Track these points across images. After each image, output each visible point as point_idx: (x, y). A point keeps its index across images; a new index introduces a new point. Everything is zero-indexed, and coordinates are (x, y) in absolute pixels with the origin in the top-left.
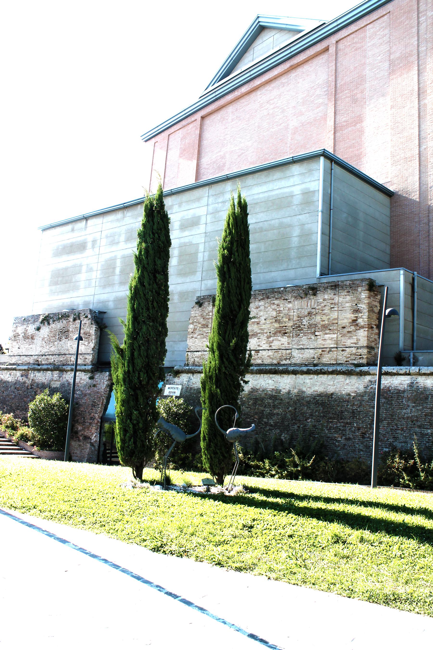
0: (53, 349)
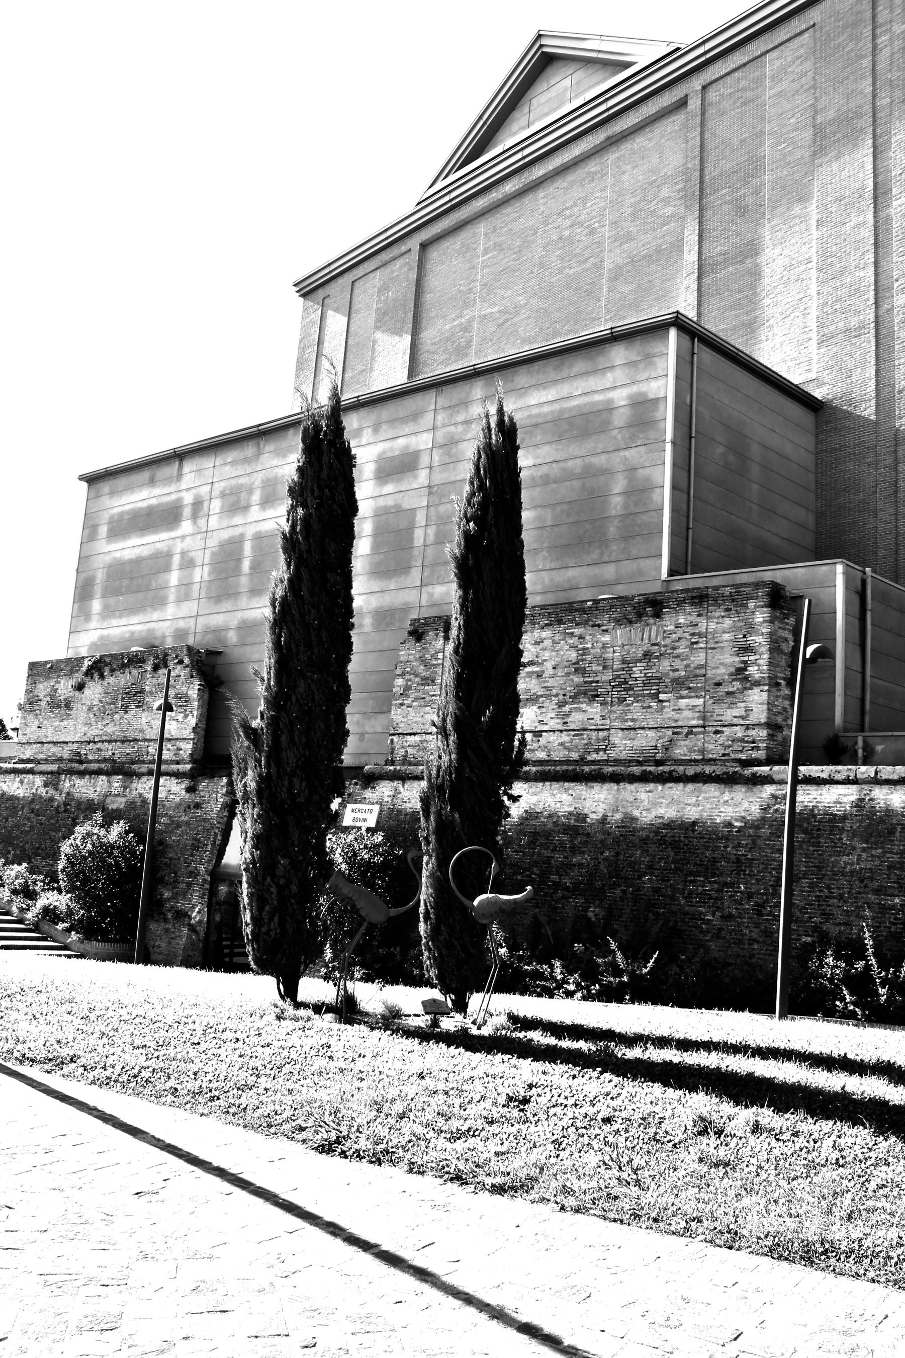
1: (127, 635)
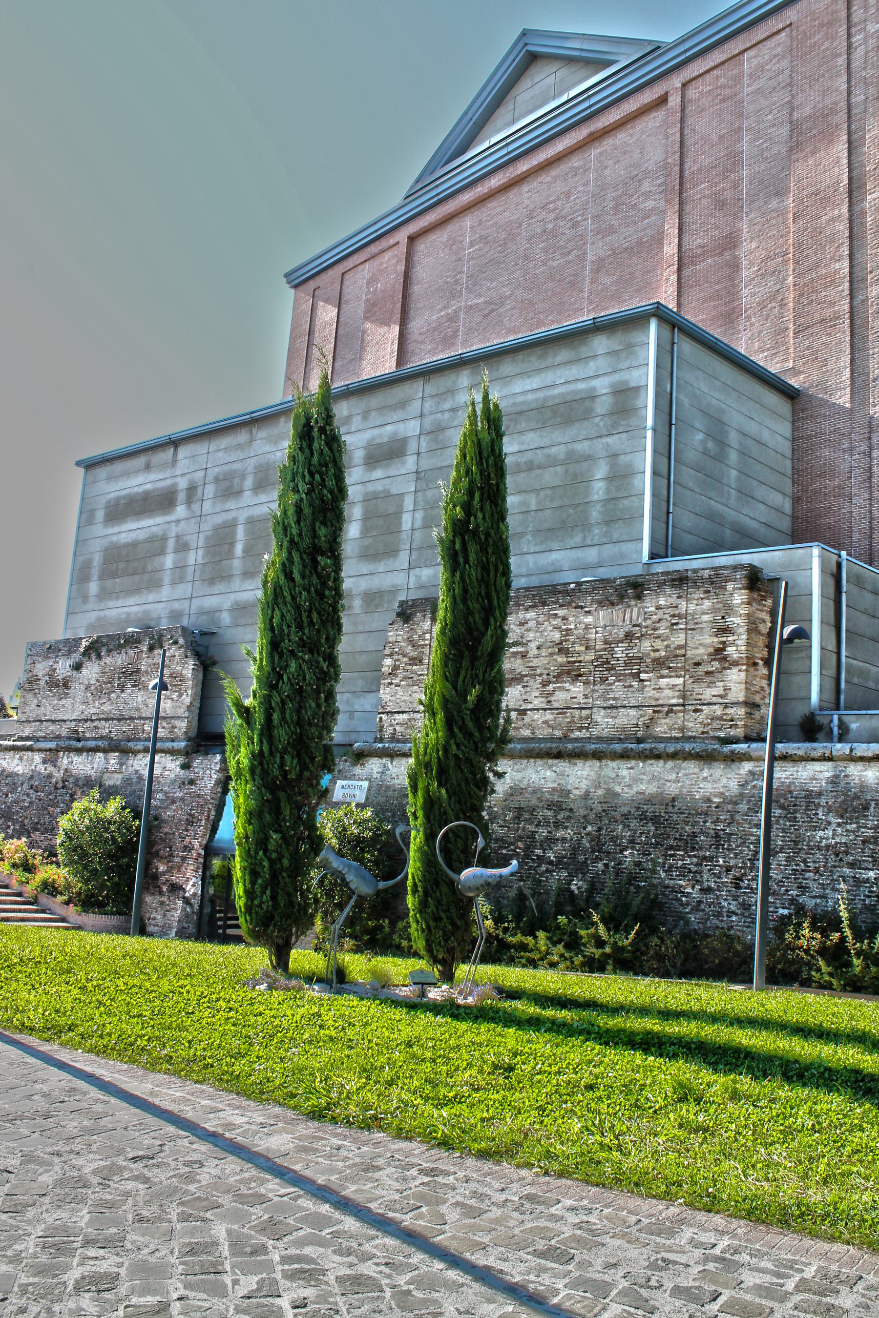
0: (107, 708)
1: (123, 617)
